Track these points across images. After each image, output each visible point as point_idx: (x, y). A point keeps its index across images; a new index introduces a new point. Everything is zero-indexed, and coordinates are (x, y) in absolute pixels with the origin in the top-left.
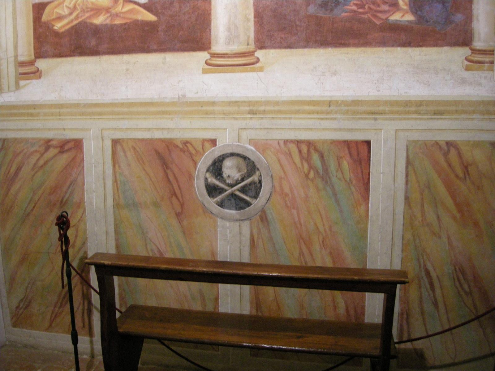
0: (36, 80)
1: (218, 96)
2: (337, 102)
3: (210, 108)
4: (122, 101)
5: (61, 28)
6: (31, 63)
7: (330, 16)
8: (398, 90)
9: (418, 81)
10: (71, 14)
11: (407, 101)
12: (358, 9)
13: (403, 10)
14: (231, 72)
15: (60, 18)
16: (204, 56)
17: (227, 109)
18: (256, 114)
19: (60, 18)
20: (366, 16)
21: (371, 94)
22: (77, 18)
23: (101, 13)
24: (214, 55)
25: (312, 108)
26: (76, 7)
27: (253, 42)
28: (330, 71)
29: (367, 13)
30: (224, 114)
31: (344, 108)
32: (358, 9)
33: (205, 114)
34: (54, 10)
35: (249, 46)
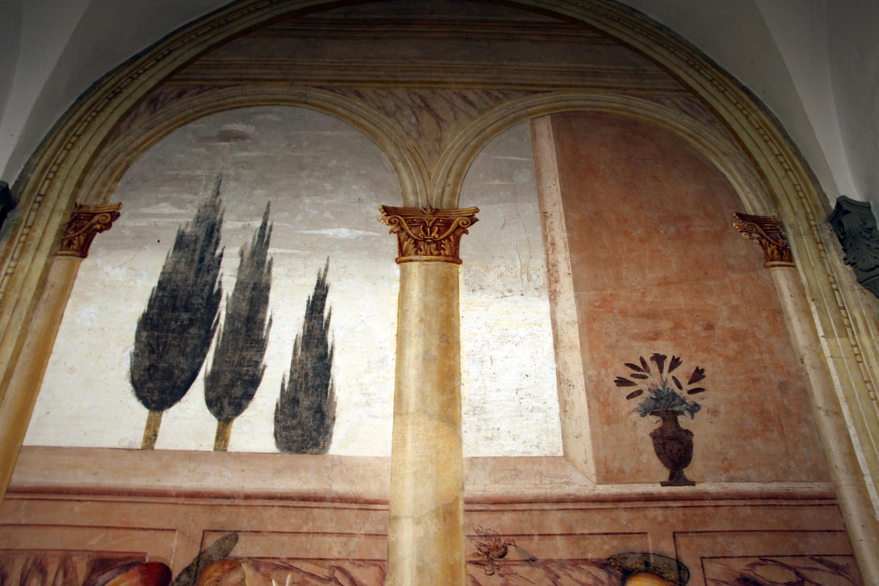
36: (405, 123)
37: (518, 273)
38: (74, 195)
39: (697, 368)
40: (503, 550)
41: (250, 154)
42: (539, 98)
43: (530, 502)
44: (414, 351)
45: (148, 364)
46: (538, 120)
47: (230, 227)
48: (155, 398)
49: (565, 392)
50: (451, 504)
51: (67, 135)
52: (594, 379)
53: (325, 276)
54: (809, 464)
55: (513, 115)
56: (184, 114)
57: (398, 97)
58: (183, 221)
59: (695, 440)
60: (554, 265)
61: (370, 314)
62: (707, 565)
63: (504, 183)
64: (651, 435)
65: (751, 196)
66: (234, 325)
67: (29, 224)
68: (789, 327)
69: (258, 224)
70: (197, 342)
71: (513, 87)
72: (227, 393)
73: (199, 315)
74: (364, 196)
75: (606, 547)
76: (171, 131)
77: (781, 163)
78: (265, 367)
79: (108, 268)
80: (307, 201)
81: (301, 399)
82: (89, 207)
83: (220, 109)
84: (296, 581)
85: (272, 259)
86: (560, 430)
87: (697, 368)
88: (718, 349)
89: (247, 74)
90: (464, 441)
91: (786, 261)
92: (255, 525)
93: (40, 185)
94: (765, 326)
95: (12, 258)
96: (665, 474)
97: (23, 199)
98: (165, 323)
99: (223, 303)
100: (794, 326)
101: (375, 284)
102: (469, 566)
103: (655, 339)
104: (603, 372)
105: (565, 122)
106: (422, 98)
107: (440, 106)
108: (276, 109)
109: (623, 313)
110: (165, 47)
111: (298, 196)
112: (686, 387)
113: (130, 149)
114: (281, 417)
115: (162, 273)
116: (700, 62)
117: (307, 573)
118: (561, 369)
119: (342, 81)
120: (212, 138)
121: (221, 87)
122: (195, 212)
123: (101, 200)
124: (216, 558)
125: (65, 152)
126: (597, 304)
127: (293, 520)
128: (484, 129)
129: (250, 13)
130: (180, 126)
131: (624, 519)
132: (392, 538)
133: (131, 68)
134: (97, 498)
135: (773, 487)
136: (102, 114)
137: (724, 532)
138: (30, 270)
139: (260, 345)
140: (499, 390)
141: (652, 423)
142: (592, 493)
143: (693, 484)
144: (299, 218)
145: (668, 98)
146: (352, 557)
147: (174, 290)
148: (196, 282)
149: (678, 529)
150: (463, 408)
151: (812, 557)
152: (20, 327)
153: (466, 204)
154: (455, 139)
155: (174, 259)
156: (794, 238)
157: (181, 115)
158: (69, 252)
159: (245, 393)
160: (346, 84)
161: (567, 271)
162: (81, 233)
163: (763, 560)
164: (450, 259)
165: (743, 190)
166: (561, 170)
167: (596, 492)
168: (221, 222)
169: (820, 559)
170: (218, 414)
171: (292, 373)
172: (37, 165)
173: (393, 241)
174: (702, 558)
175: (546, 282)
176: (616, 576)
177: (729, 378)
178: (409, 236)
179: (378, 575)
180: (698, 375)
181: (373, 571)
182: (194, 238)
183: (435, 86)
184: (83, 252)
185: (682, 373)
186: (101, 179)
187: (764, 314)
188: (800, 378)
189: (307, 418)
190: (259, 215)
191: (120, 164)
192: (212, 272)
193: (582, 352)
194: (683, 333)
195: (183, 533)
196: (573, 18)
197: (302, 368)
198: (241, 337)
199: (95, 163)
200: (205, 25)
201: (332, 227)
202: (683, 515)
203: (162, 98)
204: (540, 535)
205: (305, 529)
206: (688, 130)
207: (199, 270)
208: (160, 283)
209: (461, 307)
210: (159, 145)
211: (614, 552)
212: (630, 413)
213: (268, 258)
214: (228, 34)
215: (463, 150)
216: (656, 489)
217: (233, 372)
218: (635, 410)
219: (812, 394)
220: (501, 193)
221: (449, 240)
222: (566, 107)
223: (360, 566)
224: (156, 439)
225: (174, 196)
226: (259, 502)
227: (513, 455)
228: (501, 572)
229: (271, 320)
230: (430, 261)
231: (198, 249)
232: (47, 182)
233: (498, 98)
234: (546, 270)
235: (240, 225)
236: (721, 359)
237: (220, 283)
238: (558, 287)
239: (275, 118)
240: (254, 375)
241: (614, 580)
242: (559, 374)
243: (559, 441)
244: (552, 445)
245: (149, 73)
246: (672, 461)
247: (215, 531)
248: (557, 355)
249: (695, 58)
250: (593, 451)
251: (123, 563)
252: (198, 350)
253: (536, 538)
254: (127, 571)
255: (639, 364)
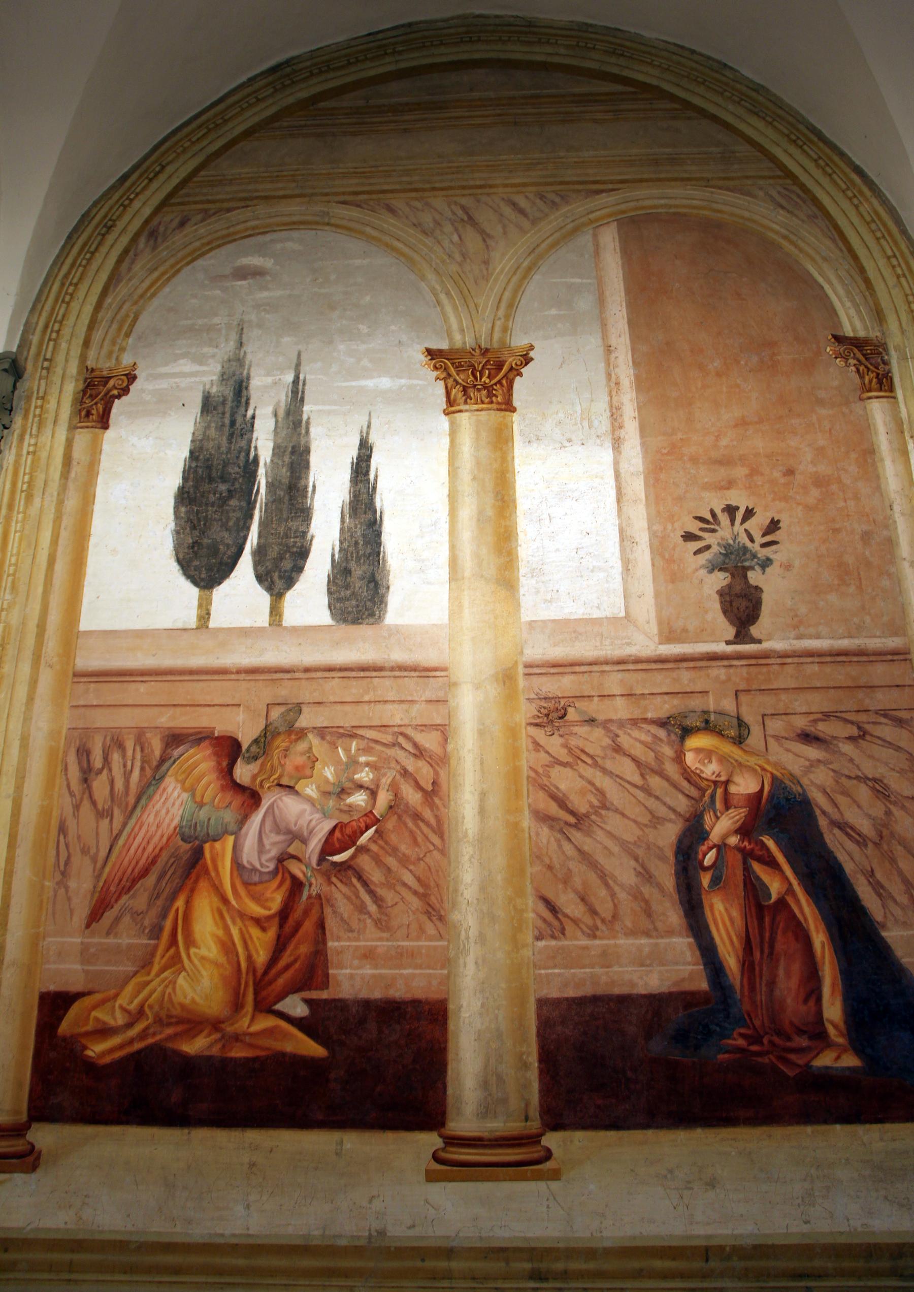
0: (23, 1175)
1: (461, 1235)
2: (721, 1248)
3: (442, 1264)
4: (234, 1241)
5: (103, 1054)
6: (18, 1131)
7: (695, 1059)
8: (848, 1220)
9: (886, 1198)
10: (129, 1025)
11: (869, 1244)
12: (749, 1045)
13: (837, 1045)
14: (488, 1180)
15: (104, 1032)
16: (430, 1141)
17: (479, 1266)
18: (546, 1280)
19: (104, 1032)
20: (766, 1060)
21: (793, 1229)
22: (143, 1035)
23: (201, 1031)
24: (452, 1141)
25: (668, 1264)
26: (144, 1011)
27: (537, 1114)
28: (701, 1179)
29: (768, 1053)
30: (474, 1278)
31: (738, 1264)
32: (749, 1045)
33: (431, 1278)
34: (89, 1015)
35: (528, 1123)
36: (446, 243)
37: (579, 419)
38: (83, 358)
39: (773, 519)
40: (563, 711)
41: (271, 294)
42: (604, 199)
43: (590, 664)
44: (467, 511)
45: (191, 541)
46: (602, 229)
47: (259, 383)
48: (203, 576)
49: (628, 550)
50: (510, 669)
51: (63, 284)
52: (659, 534)
53: (368, 433)
54: (885, 619)
55: (572, 225)
56: (191, 247)
57: (436, 210)
58: (207, 379)
59: (765, 597)
60: (618, 409)
61: (420, 471)
62: (768, 722)
63: (562, 313)
64: (718, 592)
65: (852, 312)
66: (275, 494)
67: (41, 394)
68: (880, 470)
69: (289, 378)
70: (238, 514)
71: (572, 187)
72: (277, 567)
73: (237, 486)
74: (404, 338)
75: (667, 706)
76: (178, 271)
77: (894, 267)
78: (313, 537)
79: (134, 440)
80: (342, 347)
81: (353, 569)
82: (101, 370)
83: (230, 239)
84: (361, 747)
85: (309, 418)
86: (622, 590)
87: (773, 519)
88: (798, 497)
89: (256, 191)
90: (522, 604)
91: (885, 391)
92: (316, 697)
93: (44, 347)
94: (853, 469)
95: (31, 435)
96: (731, 632)
97: (29, 366)
98: (203, 496)
99: (261, 471)
100: (887, 467)
101: (422, 440)
102: (529, 728)
103: (728, 489)
104: (669, 527)
105: (635, 228)
106: (463, 208)
107: (485, 217)
108: (295, 234)
109: (694, 460)
110: (156, 161)
111: (331, 342)
112: (759, 540)
113: (136, 297)
114: (334, 589)
115: (192, 441)
116: (804, 135)
117: (372, 740)
118: (624, 525)
119: (369, 193)
120: (225, 277)
121: (229, 210)
122: (219, 368)
123: (114, 361)
124: (282, 729)
125: (64, 305)
126: (665, 451)
127: (355, 689)
128: (538, 245)
129: (251, 106)
130: (188, 264)
131: (686, 678)
132: (452, 703)
133: (121, 191)
134: (159, 678)
135: (844, 643)
136: (97, 254)
137: (788, 689)
138: (51, 447)
139: (305, 514)
140: (558, 550)
141: (721, 579)
142: (654, 653)
143: (760, 642)
144: (334, 368)
145: (761, 189)
146: (414, 722)
147: (208, 460)
148: (230, 448)
149: (741, 688)
150: (521, 571)
151: (877, 712)
152: (53, 511)
153: (519, 341)
154: (505, 260)
155: (202, 424)
156: (898, 363)
157: (187, 250)
158: (90, 424)
159: (295, 566)
160: (374, 196)
161: (633, 415)
162: (99, 400)
163: (827, 716)
164: (503, 407)
165: (843, 305)
166: (628, 291)
167: (658, 652)
168: (248, 378)
169: (885, 713)
170: (269, 589)
171: (341, 542)
172: (37, 323)
173: (439, 389)
174: (764, 715)
175: (609, 428)
176: (676, 734)
177: (807, 529)
178: (457, 383)
179: (440, 739)
180: (774, 526)
181: (435, 736)
182: (221, 399)
183: (479, 191)
184: (104, 422)
185: (756, 525)
186: (109, 337)
187: (853, 456)
188: (886, 527)
189: (360, 587)
190: (289, 368)
191: (127, 316)
192: (246, 437)
193: (647, 505)
194: (759, 480)
195: (248, 708)
196: (645, 84)
197: (352, 536)
198: (285, 507)
199: (100, 316)
200: (200, 127)
201: (372, 378)
202: (747, 673)
203: (162, 229)
204: (599, 696)
205: (366, 698)
206: (783, 231)
207: (231, 435)
208: (191, 452)
209: (517, 461)
210: (167, 290)
211: (674, 711)
212: (697, 570)
213: (305, 417)
214: (230, 137)
215: (515, 273)
216: (720, 647)
217: (280, 544)
218: (702, 566)
219: (898, 544)
220: (559, 325)
221: (502, 385)
222: (636, 209)
223: (423, 731)
224: (209, 618)
225: (193, 350)
226: (319, 674)
227: (572, 617)
228: (561, 733)
229: (314, 486)
230: (482, 410)
231: (227, 409)
232: (52, 343)
233: (554, 203)
234: (609, 414)
235: (269, 380)
236: (800, 507)
237: (256, 448)
238: (622, 433)
239: (296, 246)
240: (302, 546)
241: (673, 737)
242: (621, 531)
243: (620, 602)
244: (614, 606)
245: (142, 198)
246: (739, 619)
247: (279, 704)
248: (620, 509)
249: (798, 130)
250: (656, 611)
251: (194, 737)
252: (241, 523)
253: (596, 699)
254: (199, 745)
255: (709, 517)
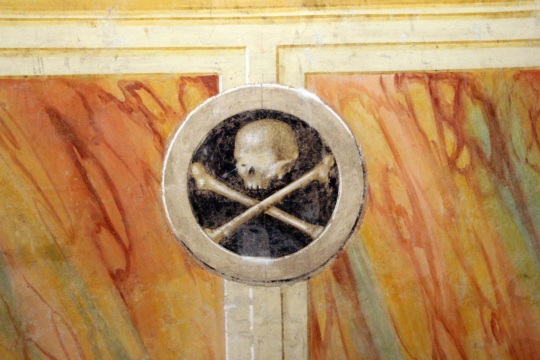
33: (187, 8)
